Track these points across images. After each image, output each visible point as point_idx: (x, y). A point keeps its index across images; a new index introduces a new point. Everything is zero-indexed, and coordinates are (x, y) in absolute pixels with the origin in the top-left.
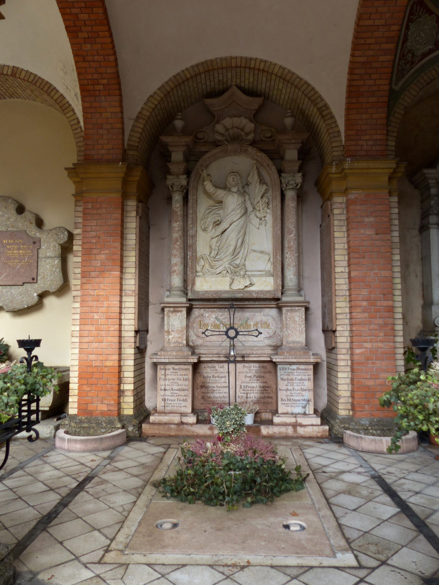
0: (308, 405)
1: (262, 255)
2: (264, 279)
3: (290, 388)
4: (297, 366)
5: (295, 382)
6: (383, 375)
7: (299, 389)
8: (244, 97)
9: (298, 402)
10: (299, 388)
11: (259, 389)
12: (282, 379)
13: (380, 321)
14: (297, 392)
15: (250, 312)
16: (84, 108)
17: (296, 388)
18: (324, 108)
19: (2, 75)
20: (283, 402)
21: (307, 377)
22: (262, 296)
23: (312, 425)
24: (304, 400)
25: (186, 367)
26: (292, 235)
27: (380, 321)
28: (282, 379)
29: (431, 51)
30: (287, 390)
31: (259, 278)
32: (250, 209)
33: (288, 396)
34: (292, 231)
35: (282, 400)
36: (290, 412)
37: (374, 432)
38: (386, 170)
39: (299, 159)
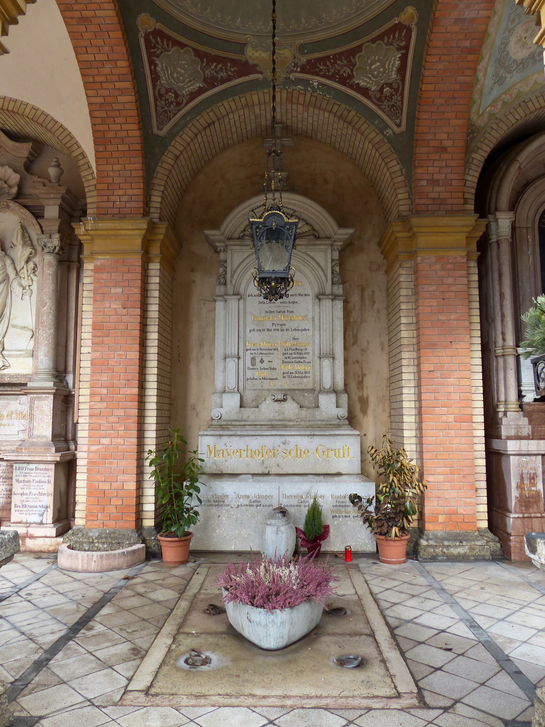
0: (45, 513)
1: (23, 331)
2: (21, 359)
3: (26, 491)
4: (36, 465)
5: (32, 484)
6: (121, 477)
7: (37, 493)
8: (10, 143)
9: (35, 509)
10: (36, 492)
11: (5, 493)
12: (17, 481)
13: (121, 412)
14: (34, 497)
15: (4, 399)
16: (96, 152)
17: (33, 491)
18: (80, 157)
19: (1, 111)
20: (17, 509)
21: (46, 479)
22: (15, 381)
23: (46, 537)
24: (42, 506)
25: (47, 466)
26: (45, 308)
27: (121, 412)
28: (17, 481)
29: (201, 91)
30: (22, 494)
31: (15, 359)
32: (12, 275)
33: (23, 501)
34: (46, 303)
35: (16, 506)
36: (24, 521)
37: (101, 546)
38: (136, 232)
39: (59, 218)
